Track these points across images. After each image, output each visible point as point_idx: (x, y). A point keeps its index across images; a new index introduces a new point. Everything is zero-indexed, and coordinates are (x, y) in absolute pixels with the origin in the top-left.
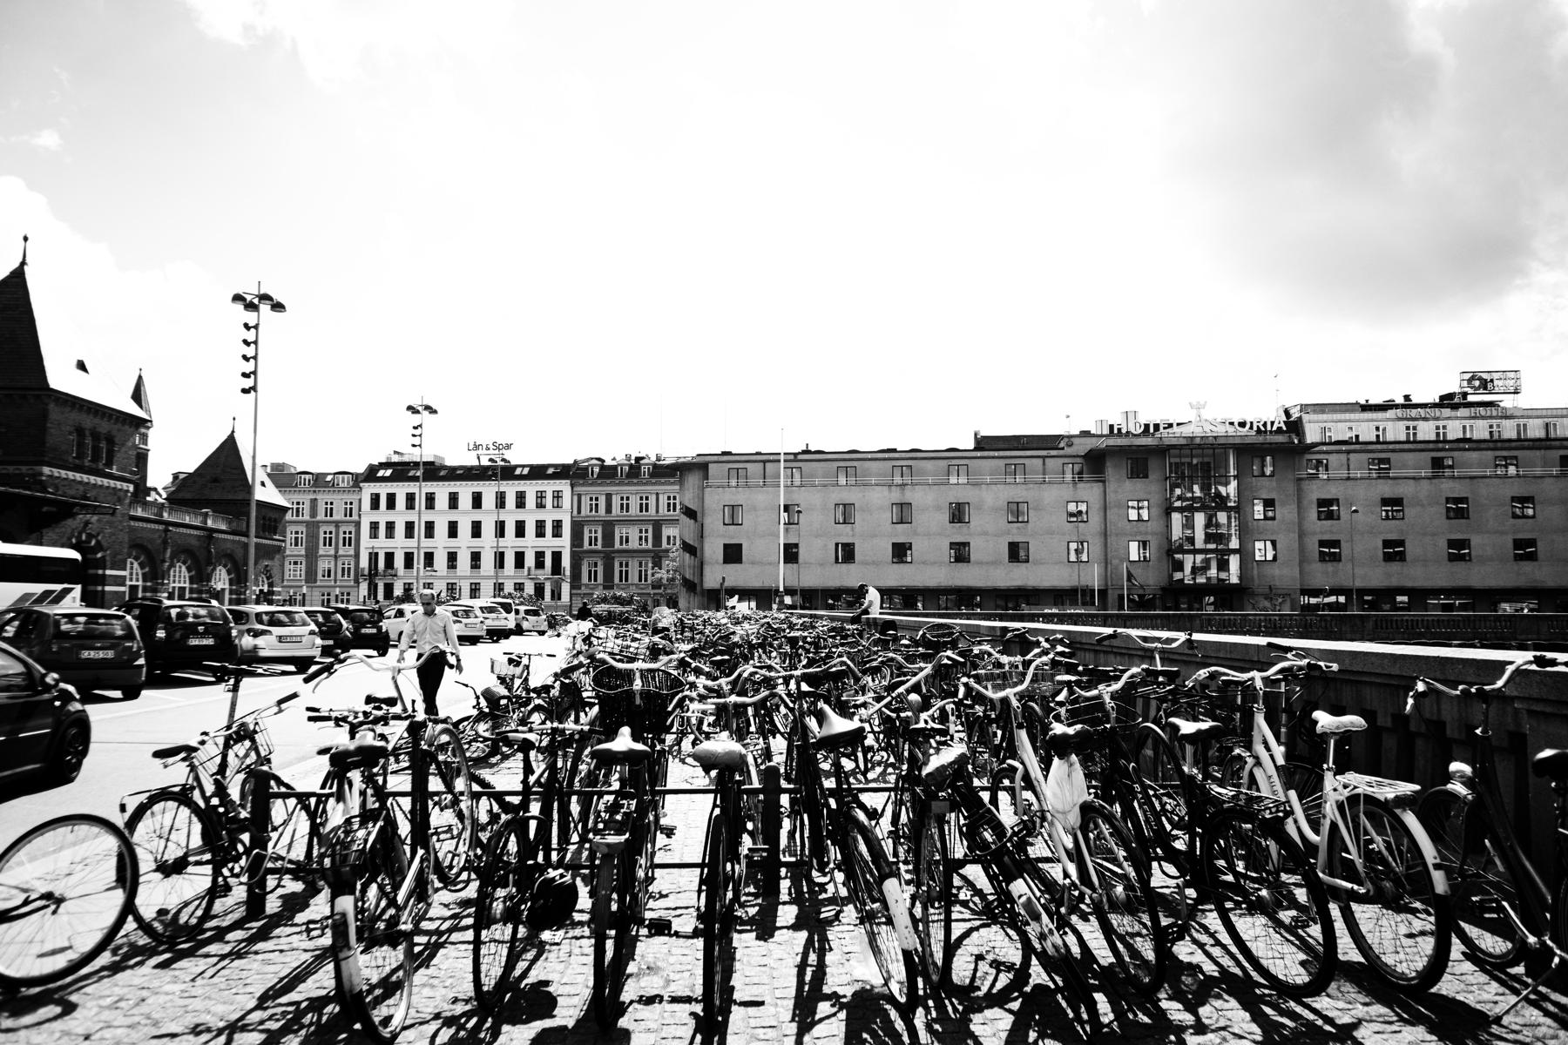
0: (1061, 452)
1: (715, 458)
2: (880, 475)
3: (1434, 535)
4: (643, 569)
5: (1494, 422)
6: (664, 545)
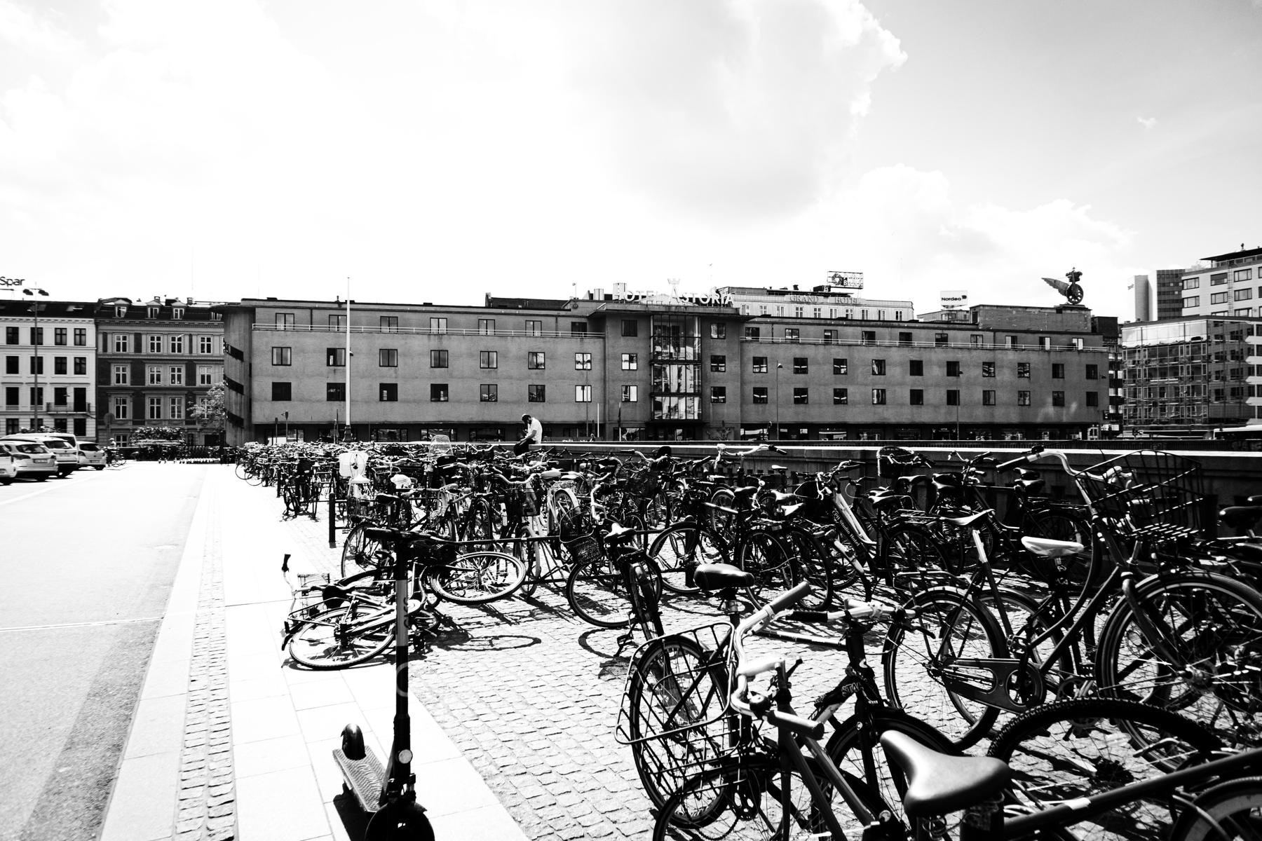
0: (569, 313)
1: (261, 303)
2: (419, 326)
3: (825, 385)
4: (155, 406)
5: (849, 308)
6: (199, 383)
